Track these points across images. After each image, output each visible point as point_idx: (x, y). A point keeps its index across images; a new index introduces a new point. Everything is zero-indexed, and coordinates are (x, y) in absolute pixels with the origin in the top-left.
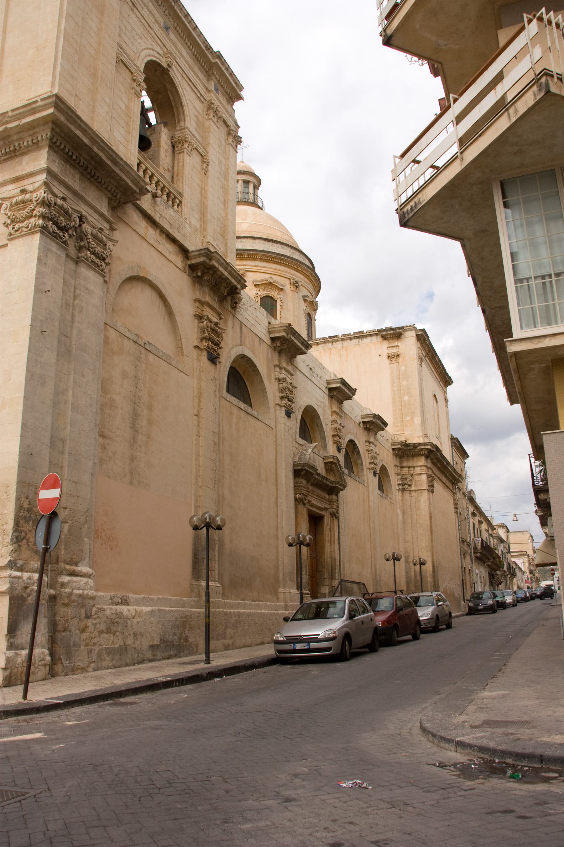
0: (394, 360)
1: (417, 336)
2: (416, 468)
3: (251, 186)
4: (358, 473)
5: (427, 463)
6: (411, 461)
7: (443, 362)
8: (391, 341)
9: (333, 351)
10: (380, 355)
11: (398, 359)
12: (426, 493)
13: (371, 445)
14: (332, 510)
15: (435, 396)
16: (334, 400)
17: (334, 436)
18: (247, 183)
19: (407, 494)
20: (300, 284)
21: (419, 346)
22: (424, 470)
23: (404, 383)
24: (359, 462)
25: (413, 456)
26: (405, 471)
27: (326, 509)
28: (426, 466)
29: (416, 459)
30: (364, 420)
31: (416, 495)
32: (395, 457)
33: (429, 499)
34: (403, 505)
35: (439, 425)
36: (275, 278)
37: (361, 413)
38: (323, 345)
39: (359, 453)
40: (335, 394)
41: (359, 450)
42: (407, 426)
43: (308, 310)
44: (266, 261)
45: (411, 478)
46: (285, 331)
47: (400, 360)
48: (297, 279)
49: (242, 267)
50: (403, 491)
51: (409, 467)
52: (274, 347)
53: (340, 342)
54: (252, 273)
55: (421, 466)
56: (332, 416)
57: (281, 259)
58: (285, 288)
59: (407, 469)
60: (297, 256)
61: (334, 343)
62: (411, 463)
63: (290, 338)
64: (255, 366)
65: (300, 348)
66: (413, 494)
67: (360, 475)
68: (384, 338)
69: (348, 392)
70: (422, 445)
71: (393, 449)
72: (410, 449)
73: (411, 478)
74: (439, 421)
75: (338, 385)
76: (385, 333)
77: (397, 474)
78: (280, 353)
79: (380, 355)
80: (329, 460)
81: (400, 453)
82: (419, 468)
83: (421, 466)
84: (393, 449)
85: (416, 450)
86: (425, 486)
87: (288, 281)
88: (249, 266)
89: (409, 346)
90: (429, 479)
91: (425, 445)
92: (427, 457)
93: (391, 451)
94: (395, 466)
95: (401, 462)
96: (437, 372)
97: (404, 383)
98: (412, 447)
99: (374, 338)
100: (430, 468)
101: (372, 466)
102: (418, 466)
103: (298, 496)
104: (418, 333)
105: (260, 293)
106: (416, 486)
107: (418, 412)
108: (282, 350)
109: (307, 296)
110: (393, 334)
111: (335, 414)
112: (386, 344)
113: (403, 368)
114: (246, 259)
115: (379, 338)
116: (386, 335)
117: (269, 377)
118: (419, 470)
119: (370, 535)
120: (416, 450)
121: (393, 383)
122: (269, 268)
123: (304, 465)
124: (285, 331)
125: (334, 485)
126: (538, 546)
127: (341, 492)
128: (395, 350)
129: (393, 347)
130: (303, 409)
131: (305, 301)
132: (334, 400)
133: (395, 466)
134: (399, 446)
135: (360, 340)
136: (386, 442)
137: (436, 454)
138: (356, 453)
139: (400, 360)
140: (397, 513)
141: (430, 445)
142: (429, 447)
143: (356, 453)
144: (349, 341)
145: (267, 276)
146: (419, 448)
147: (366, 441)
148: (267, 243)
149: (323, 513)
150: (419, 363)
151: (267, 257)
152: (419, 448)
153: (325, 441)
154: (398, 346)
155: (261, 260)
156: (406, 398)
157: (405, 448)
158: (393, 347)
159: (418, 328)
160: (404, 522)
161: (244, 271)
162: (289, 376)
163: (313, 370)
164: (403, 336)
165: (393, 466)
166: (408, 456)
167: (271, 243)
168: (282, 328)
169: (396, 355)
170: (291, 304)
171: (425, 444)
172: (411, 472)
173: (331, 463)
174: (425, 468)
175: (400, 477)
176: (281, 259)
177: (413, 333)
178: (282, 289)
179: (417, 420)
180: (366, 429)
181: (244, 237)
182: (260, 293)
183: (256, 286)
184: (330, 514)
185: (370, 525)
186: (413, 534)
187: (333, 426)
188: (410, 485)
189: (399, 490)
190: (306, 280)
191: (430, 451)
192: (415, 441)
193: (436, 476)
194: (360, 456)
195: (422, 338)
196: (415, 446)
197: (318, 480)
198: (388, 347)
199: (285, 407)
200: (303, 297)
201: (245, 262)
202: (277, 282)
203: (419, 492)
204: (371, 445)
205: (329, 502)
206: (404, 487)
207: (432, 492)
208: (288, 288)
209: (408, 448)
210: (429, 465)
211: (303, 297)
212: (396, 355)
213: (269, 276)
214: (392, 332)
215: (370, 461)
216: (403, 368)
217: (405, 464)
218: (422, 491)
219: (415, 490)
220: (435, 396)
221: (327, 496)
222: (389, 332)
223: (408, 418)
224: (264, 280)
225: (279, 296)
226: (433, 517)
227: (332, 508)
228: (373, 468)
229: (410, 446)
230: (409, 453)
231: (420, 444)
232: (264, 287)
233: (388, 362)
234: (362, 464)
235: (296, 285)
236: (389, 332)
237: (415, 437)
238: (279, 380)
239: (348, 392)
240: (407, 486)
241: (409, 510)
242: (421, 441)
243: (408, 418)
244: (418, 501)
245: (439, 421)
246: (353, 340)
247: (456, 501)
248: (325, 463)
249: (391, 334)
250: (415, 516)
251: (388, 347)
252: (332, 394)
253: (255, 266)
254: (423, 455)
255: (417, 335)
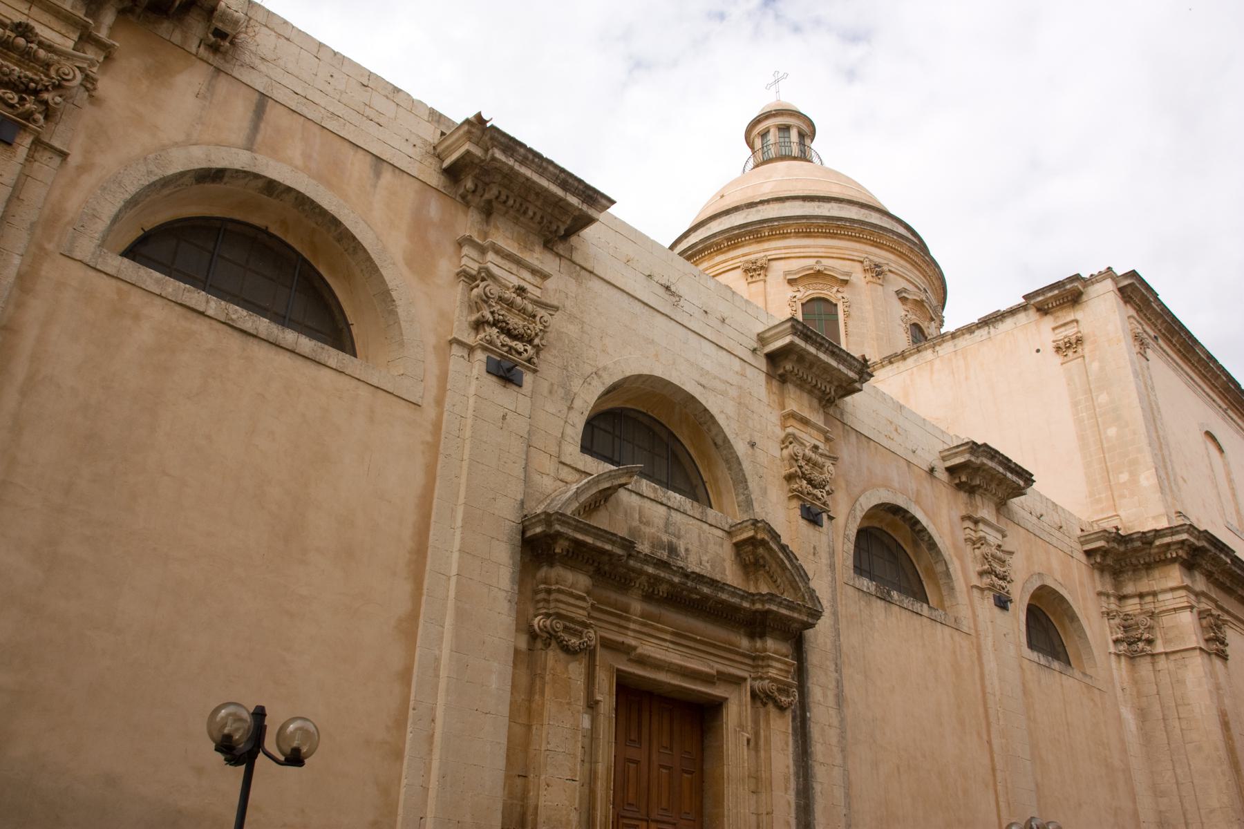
0: (1070, 353)
1: (1121, 290)
2: (1161, 597)
3: (794, 135)
4: (941, 601)
5: (1194, 581)
6: (1145, 581)
7: (1221, 362)
8: (1059, 314)
9: (937, 363)
10: (1038, 351)
11: (1079, 349)
12: (1197, 662)
13: (981, 526)
14: (757, 684)
15: (1209, 434)
16: (790, 387)
17: (789, 478)
18: (785, 129)
19: (1145, 666)
20: (885, 268)
21: (1132, 312)
22: (1181, 598)
23: (1103, 398)
24: (939, 568)
25: (1149, 567)
26: (1132, 606)
27: (738, 681)
28: (1186, 588)
29: (1156, 573)
30: (949, 464)
31: (1172, 665)
32: (1097, 575)
33: (1213, 674)
34: (1139, 694)
35: (1237, 504)
36: (825, 262)
37: (941, 447)
38: (915, 357)
39: (932, 545)
40: (789, 367)
41: (930, 537)
42: (1122, 496)
43: (914, 319)
44: (808, 235)
45: (1150, 622)
46: (469, 136)
47: (1087, 349)
48: (877, 260)
49: (762, 254)
50: (1132, 657)
51: (1141, 596)
52: (463, 197)
53: (950, 343)
54: (782, 262)
55: (1173, 589)
56: (784, 427)
57: (838, 227)
58: (853, 279)
59: (1136, 600)
60: (875, 218)
61: (937, 348)
62: (1145, 585)
63: (494, 159)
64: (335, 222)
65: (561, 199)
66: (1162, 663)
67: (947, 604)
68: (1043, 310)
69: (834, 363)
70: (1165, 536)
71: (1089, 553)
72: (1135, 550)
73: (1150, 622)
74: (1234, 495)
75: (787, 340)
76: (1040, 298)
77: (1108, 615)
78: (488, 212)
79: (1038, 351)
80: (745, 536)
81: (1109, 561)
82: (1169, 596)
83: (1173, 589)
84: (1089, 553)
85: (1154, 551)
86: (1194, 638)
87: (858, 265)
88: (775, 249)
89: (1104, 316)
90: (1204, 622)
91: (1173, 534)
92: (1189, 566)
93: (1083, 558)
94: (1100, 594)
95: (1118, 585)
96: (1213, 387)
97: (1103, 398)
98: (1138, 544)
99: (1021, 317)
100: (1203, 594)
101: (986, 580)
102: (1164, 591)
103: (537, 622)
104: (1121, 285)
105: (799, 295)
106: (1167, 642)
107: (1147, 458)
108: (489, 202)
109: (905, 290)
110: (1065, 296)
111: (791, 422)
112: (1048, 322)
113: (1095, 366)
114: (770, 238)
115: (1032, 314)
116: (1045, 301)
117: (421, 263)
118: (1168, 600)
119: (994, 770)
120: (1154, 551)
121: (1075, 404)
122: (814, 246)
123: (548, 518)
124: (469, 136)
125: (758, 606)
126: (873, 589)
127: (809, 633)
128: (1070, 332)
129: (1065, 325)
130: (609, 381)
131: (903, 300)
132: (790, 387)
133: (1100, 594)
134: (1101, 543)
135: (992, 329)
136: (1057, 534)
137: (1215, 559)
138: (924, 546)
139: (1086, 350)
140: (1119, 717)
141: (1187, 532)
142: (1184, 536)
143: (924, 546)
144: (967, 336)
145: (811, 262)
146: (1157, 543)
147: (964, 518)
148: (807, 204)
149: (718, 691)
150: (1137, 349)
151: (808, 227)
152: (1157, 543)
153: (747, 488)
154: (1077, 321)
155: (798, 234)
156: (1112, 432)
157: (1122, 549)
158: (1065, 325)
159: (1119, 273)
160: (1147, 738)
161: (764, 261)
162: (537, 281)
163: (673, 289)
164: (1084, 298)
165: (1091, 595)
166: (1135, 569)
167: (817, 203)
168: (461, 132)
169: (1073, 341)
170: (869, 307)
171: (1172, 531)
172: (1147, 607)
173: (752, 541)
174: (1183, 593)
175: (1117, 621)
176: (838, 227)
177: (1108, 284)
178: (845, 282)
179: (1147, 479)
180: (960, 486)
181: (762, 202)
182: (799, 295)
183: (791, 282)
184: (754, 695)
185: (989, 742)
186: (1179, 771)
187: (785, 452)
188: (1150, 642)
189: (1118, 655)
190: (902, 262)
191: (1195, 552)
192: (1148, 526)
193: (1228, 612)
194: (939, 552)
195: (1136, 292)
196: (1147, 539)
197: (672, 584)
198: (1054, 329)
199: (485, 349)
200: (898, 293)
201: (766, 245)
202: (833, 269)
203: (1178, 656)
204: (981, 526)
205: (754, 659)
206: (1134, 647)
207: (1223, 656)
208: (858, 276)
209: (1129, 546)
210: (1200, 584)
211: (898, 293)
212: (1073, 341)
213: (811, 262)
214: (1056, 292)
215: (979, 568)
216: (1095, 366)
217: (1129, 589)
218: (1184, 654)
219: (1166, 654)
220: (1209, 434)
221: (745, 643)
222: (1050, 295)
223: (1124, 477)
224: (804, 269)
225: (839, 295)
226: (1232, 725)
227: (761, 678)
228: (991, 587)
229: (1132, 540)
230: (1134, 561)
231: (1158, 533)
232: (806, 282)
233: (1058, 359)
234: (947, 574)
235: (877, 271)
236: (1050, 295)
237: (1143, 513)
238: (470, 279)
239: (834, 363)
240: (1141, 645)
241: (1157, 707)
242: (1163, 524)
243: (1124, 477)
244: (1181, 682)
245: (1234, 495)
246: (977, 333)
247: (1214, 646)
248: (738, 546)
249: (1055, 297)
250: (1177, 723)
251: (1054, 329)
252: (781, 371)
253: (786, 248)
254: (1173, 561)
255: (1121, 290)
